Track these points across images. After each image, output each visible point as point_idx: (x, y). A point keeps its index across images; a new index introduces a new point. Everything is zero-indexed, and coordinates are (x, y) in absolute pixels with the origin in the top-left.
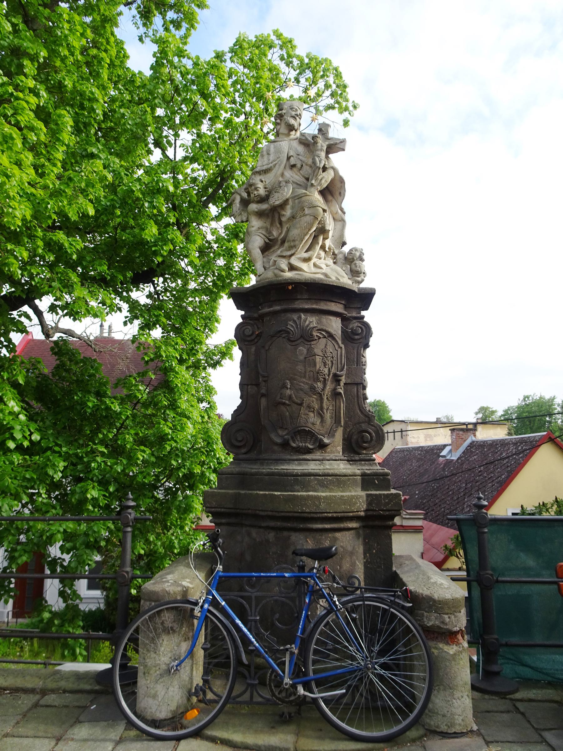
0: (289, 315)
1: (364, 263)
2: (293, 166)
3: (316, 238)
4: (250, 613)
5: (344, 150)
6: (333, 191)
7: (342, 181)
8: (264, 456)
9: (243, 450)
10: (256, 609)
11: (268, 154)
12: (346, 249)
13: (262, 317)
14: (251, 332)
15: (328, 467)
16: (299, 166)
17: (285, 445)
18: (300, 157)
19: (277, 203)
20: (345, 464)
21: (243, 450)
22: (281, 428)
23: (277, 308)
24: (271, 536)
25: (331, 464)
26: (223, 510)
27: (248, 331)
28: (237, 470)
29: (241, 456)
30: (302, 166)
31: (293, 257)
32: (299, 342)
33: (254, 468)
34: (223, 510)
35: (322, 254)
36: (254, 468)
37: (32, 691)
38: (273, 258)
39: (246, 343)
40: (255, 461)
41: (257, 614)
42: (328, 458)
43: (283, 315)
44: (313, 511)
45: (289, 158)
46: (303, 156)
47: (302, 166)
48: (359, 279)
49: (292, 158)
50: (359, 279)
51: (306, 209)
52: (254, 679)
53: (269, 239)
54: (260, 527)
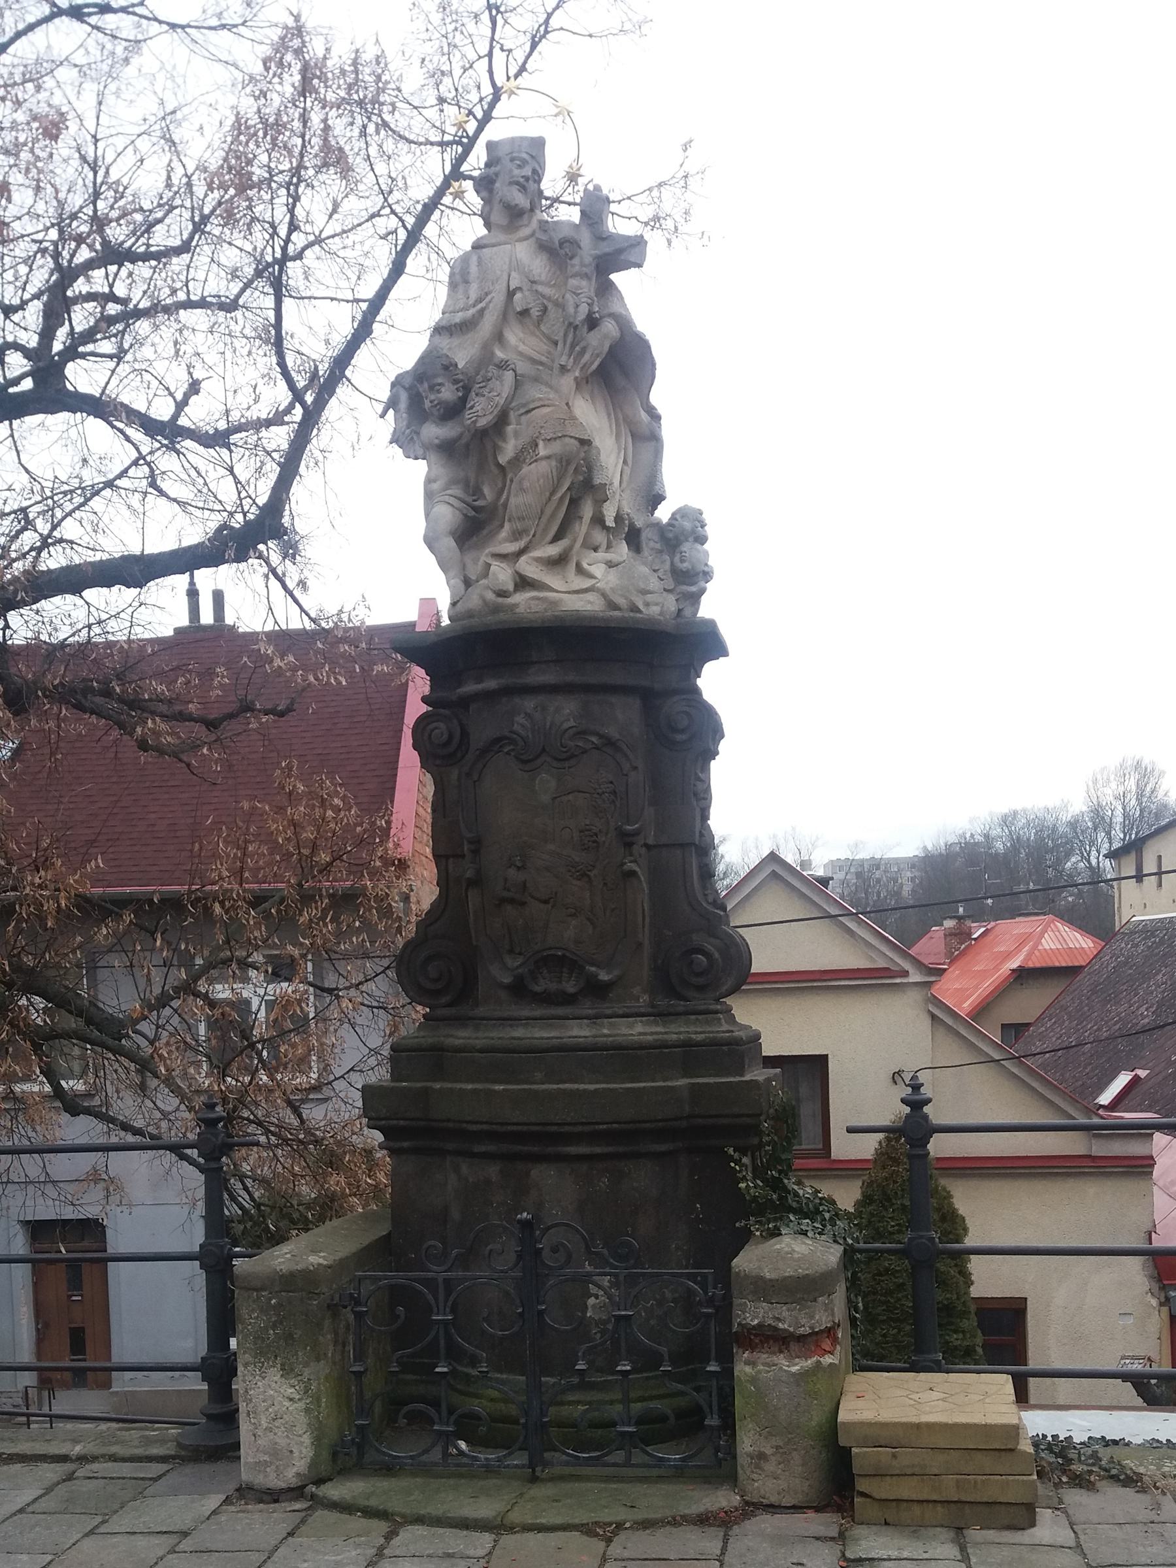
0: (517, 700)
1: (706, 546)
2: (525, 313)
3: (574, 503)
4: (435, 1310)
5: (640, 266)
6: (621, 368)
7: (642, 346)
8: (481, 1011)
9: (443, 1000)
10: (446, 1301)
11: (467, 282)
12: (663, 513)
13: (465, 702)
14: (445, 737)
15: (605, 1031)
16: (535, 312)
17: (519, 990)
18: (540, 288)
19: (482, 422)
20: (644, 1024)
21: (443, 1000)
22: (511, 952)
23: (491, 684)
24: (493, 1171)
25: (612, 1025)
26: (402, 1123)
27: (440, 730)
28: (430, 1040)
29: (441, 1012)
30: (545, 310)
31: (523, 558)
32: (539, 761)
33: (461, 1036)
34: (402, 1123)
35: (600, 537)
36: (461, 1036)
37: (63, 1459)
38: (484, 558)
39: (438, 762)
40: (461, 1021)
41: (448, 1310)
42: (609, 1012)
43: (504, 700)
44: (569, 1120)
45: (511, 294)
46: (547, 284)
47: (545, 310)
48: (693, 589)
49: (518, 296)
50: (693, 589)
51: (541, 444)
52: (447, 1424)
53: (474, 508)
54: (474, 1155)
